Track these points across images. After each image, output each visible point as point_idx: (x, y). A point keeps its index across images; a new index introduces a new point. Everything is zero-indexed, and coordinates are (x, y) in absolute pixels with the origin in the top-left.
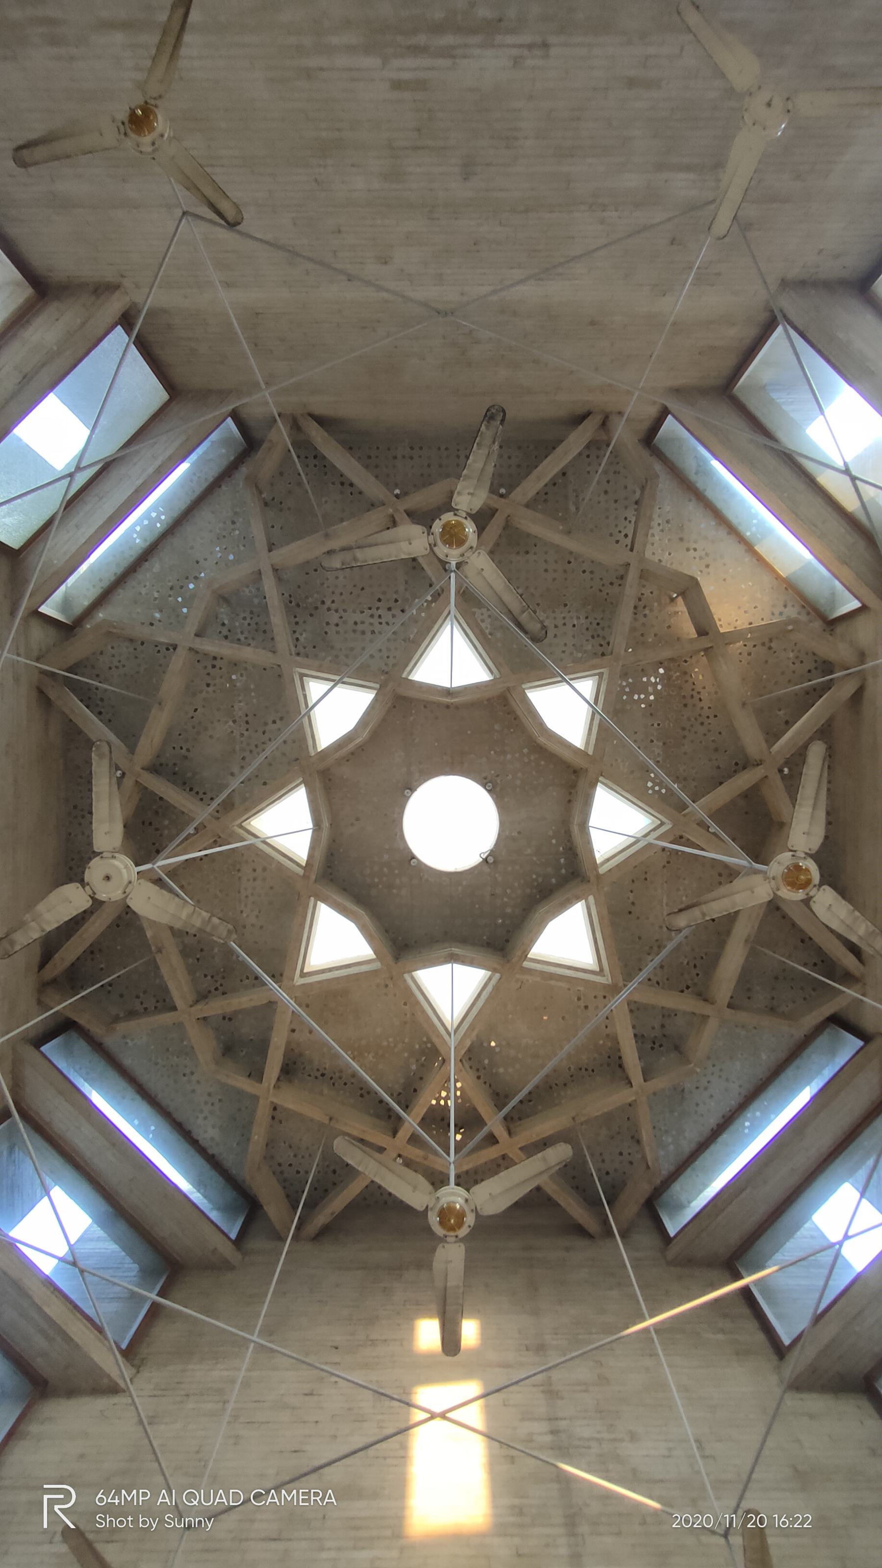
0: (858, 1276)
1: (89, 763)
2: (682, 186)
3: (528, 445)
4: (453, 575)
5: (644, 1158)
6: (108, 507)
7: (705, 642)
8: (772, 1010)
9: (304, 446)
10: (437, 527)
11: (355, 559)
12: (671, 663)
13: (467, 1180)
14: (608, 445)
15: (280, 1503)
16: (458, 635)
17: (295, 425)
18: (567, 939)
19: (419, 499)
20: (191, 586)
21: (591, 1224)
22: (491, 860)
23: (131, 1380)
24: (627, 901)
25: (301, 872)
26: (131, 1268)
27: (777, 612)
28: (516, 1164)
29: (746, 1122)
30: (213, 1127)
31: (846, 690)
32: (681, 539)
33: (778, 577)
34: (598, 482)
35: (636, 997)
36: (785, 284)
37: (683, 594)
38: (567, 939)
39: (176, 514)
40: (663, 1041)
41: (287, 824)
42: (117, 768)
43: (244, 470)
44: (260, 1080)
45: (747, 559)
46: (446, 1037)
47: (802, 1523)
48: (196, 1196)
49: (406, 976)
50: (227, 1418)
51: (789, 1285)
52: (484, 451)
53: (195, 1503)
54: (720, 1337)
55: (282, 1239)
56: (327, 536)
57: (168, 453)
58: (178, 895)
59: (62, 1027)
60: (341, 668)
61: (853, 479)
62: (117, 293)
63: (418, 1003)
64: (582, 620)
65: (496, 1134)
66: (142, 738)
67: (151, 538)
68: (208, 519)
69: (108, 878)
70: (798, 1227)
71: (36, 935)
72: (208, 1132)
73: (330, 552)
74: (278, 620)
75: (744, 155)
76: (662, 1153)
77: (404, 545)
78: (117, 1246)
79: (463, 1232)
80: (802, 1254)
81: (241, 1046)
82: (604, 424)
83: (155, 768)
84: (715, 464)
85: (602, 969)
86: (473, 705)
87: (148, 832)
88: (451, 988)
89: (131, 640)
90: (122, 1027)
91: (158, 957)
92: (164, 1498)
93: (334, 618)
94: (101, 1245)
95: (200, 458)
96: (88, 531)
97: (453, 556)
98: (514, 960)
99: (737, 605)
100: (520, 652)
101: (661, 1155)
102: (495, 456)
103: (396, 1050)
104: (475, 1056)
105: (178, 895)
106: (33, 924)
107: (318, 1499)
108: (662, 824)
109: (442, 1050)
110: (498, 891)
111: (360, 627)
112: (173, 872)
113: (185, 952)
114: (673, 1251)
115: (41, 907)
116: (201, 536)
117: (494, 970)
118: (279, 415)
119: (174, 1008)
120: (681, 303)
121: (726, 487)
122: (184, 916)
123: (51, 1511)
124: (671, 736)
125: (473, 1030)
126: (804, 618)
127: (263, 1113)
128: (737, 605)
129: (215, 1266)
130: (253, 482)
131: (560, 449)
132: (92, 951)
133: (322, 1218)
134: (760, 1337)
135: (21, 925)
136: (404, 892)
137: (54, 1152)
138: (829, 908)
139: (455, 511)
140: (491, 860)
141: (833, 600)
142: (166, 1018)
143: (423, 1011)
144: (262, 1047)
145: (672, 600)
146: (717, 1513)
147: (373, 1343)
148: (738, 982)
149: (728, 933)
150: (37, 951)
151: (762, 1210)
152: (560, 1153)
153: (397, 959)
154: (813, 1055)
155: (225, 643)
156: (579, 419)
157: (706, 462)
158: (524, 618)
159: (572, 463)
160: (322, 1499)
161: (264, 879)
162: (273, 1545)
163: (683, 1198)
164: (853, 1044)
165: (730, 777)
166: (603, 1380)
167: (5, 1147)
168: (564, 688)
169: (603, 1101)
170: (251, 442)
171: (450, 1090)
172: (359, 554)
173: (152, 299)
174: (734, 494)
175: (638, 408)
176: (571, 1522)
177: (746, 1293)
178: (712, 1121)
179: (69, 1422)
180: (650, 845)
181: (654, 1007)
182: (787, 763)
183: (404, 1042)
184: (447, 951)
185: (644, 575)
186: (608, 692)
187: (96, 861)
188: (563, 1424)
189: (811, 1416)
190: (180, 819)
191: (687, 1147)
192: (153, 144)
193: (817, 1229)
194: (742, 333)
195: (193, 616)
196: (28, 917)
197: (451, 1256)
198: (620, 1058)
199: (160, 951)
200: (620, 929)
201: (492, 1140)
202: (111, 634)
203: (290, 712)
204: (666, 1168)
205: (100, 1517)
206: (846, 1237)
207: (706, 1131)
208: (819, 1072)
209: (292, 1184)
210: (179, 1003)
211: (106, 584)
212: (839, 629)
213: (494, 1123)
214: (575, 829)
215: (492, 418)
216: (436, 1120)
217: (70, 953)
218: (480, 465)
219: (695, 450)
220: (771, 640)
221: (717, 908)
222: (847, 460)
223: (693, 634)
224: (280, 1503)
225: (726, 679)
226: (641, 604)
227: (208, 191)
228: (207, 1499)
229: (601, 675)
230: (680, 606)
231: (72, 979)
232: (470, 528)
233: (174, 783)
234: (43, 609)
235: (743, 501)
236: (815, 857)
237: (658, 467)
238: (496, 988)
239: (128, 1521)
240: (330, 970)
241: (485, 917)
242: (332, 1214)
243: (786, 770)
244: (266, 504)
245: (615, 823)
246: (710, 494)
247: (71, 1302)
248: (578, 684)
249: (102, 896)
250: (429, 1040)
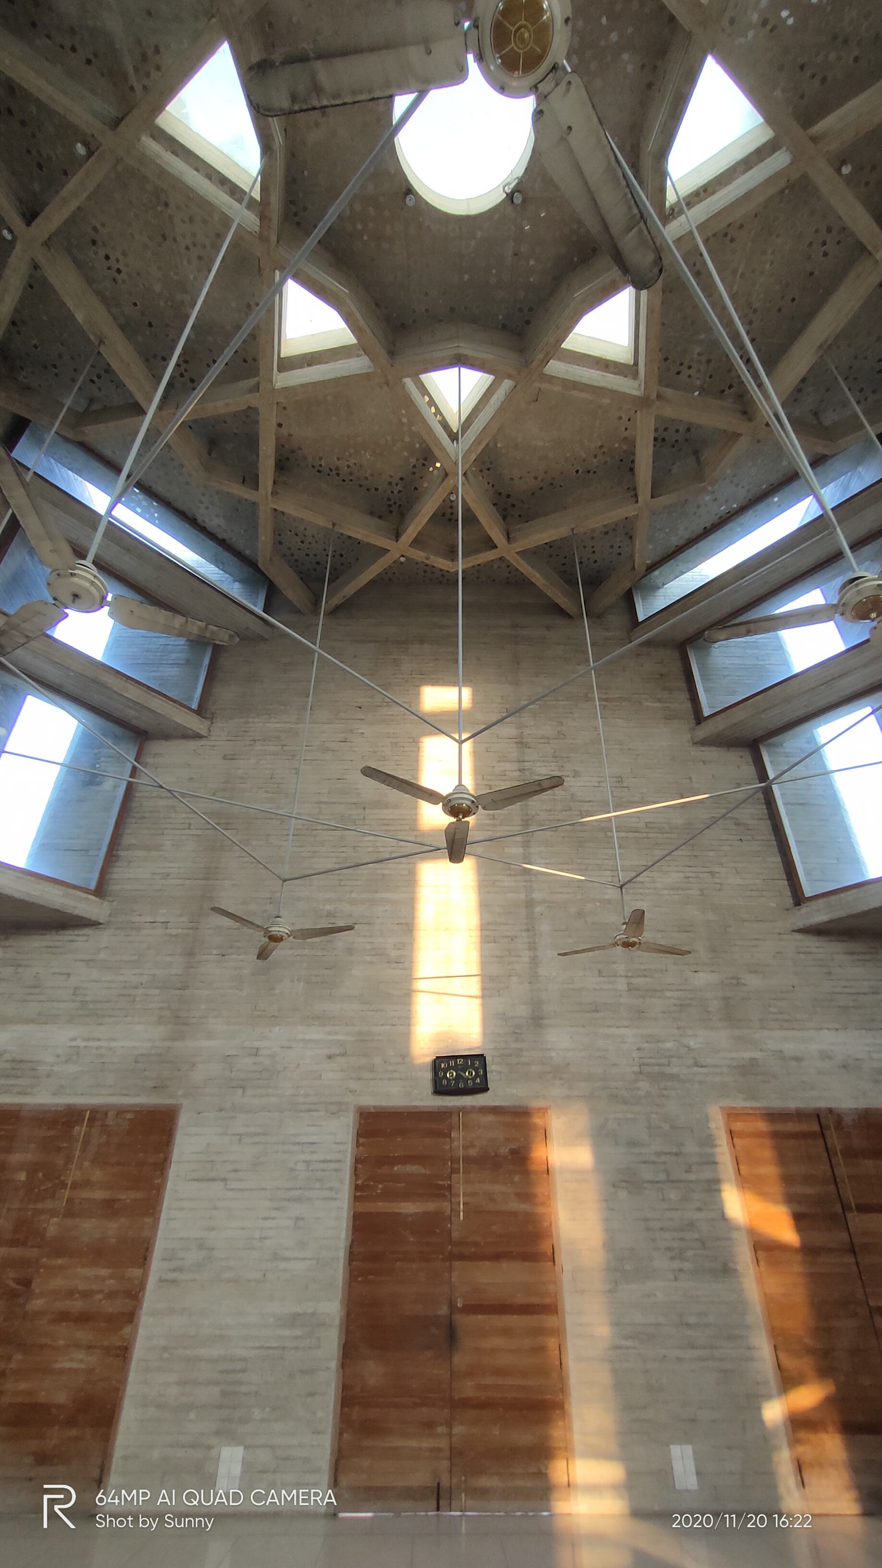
11: (317, 89)
15: (280, 1503)
30: (217, 516)
44: (256, 487)
47: (802, 1523)
51: (731, 670)
53: (195, 1503)
72: (215, 521)
91: (102, 350)
92: (164, 1498)
98: (535, 364)
103: (395, 449)
107: (318, 1499)
110: (524, 249)
123: (52, 1515)
125: (480, 444)
134: (688, 705)
144: (252, 442)
160: (322, 1500)
163: (659, 582)
166: (561, 735)
178: (707, 519)
183: (403, 441)
191: (676, 541)
198: (633, 461)
205: (100, 1518)
209: (303, 564)
224: (280, 1503)
228: (207, 1499)
239: (128, 1521)
242: (344, 597)
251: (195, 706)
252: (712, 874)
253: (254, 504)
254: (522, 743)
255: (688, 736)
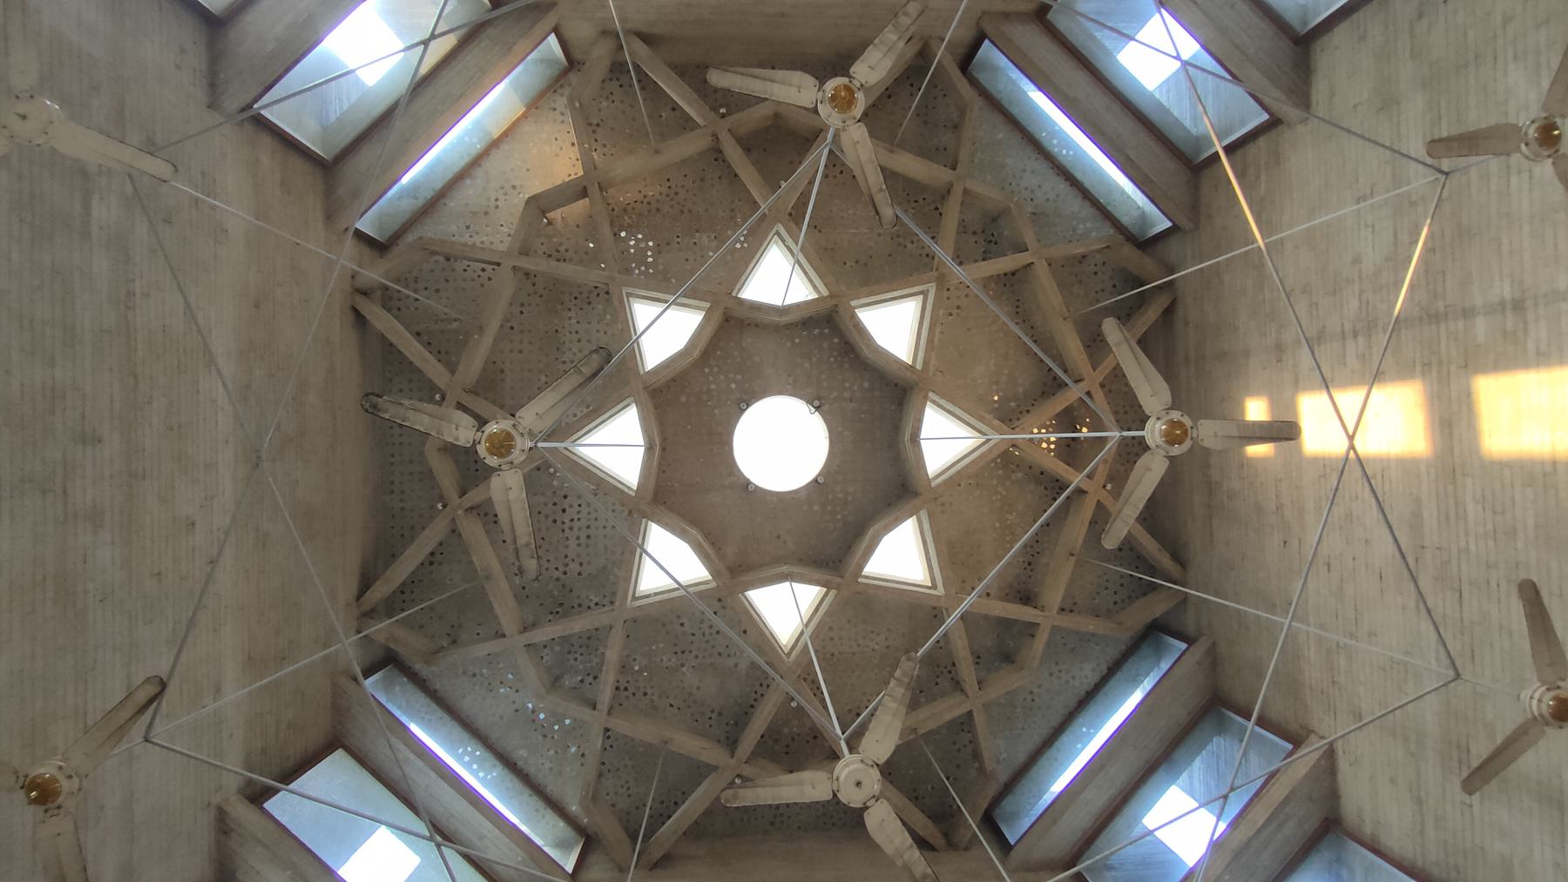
0: (1204, 47)
2: (105, 212)
3: (386, 370)
5: (1099, 251)
6: (460, 806)
7: (594, 190)
8: (956, 127)
9: (390, 607)
10: (493, 461)
11: (528, 545)
13: (1133, 415)
14: (387, 288)
16: (589, 439)
17: (369, 615)
18: (893, 326)
20: (542, 716)
21: (1164, 300)
22: (817, 403)
23: (1323, 738)
24: (855, 268)
25: (833, 592)
26: (1218, 744)
27: (561, 118)
29: (1063, 154)
31: (642, 49)
33: (524, 116)
36: (213, 105)
37: (544, 213)
38: (893, 326)
39: (465, 736)
40: (988, 233)
41: (785, 608)
42: (733, 782)
43: (418, 667)
46: (991, 444)
48: (1147, 684)
49: (933, 484)
50: (1353, 642)
51: (1214, 112)
52: (411, 414)
54: (1263, 178)
55: (1186, 597)
56: (488, 577)
58: (875, 709)
59: (990, 823)
61: (433, 37)
62: (228, 809)
64: (572, 314)
66: (703, 759)
68: (472, 702)
69: (858, 784)
71: (917, 853)
72: (1087, 674)
74: (578, 625)
75: (82, 144)
77: (512, 495)
79: (1187, 421)
81: (1002, 645)
82: (365, 293)
83: (732, 743)
84: (406, 180)
86: (662, 425)
87: (800, 745)
88: (944, 440)
89: (600, 775)
90: (989, 765)
91: (921, 732)
93: (574, 567)
94: (1196, 775)
95: (406, 713)
96: (486, 826)
97: (522, 443)
99: (555, 158)
100: (607, 376)
101: (1097, 235)
104: (1008, 417)
105: (875, 709)
106: (906, 857)
108: (778, 233)
109: (1002, 449)
110: (847, 395)
111: (583, 540)
114: (1184, 223)
115: (889, 849)
116: (487, 707)
117: (926, 398)
118: (359, 632)
119: (970, 713)
120: (235, 212)
121: (431, 168)
122: (895, 705)
126: (567, 91)
127: (1066, 621)
128: (555, 158)
129: (1213, 661)
131: (393, 339)
133: (1166, 562)
134: (1262, 141)
135: (906, 867)
136: (851, 489)
137: (1104, 833)
140: (817, 403)
141: (548, 61)
142: (979, 720)
144: (1006, 624)
145: (550, 223)
146: (1419, 179)
147: (1280, 507)
151: (1144, 137)
153: (916, 494)
154: (998, 88)
156: (360, 319)
157: (403, 190)
158: (587, 371)
162: (1466, 595)
163: (1136, 213)
164: (987, 50)
165: (729, 166)
167: (1108, 874)
170: (386, 660)
171: (1041, 437)
173: (234, 772)
174: (438, 160)
175: (347, 256)
176: (1434, 318)
177: (1229, 149)
178: (1063, 186)
179: (1370, 794)
182: (715, 109)
184: (908, 444)
185: (525, 252)
186: (647, 288)
187: (843, 798)
188: (1348, 327)
189: (1332, 95)
191: (1087, 210)
192: (70, 777)
193: (1160, 86)
194: (267, 150)
196: (899, 863)
199: (915, 730)
200: (883, 272)
202: (593, 797)
203: (675, 609)
208: (1014, 82)
210: (963, 709)
211: (541, 805)
212: (577, 55)
213: (1074, 393)
214: (785, 319)
215: (375, 407)
216: (1071, 452)
218: (426, 419)
219: (391, 199)
221: (875, 180)
222: (402, 46)
225: (634, 169)
226: (555, 254)
227: (125, 714)
229: (629, 295)
230: (556, 215)
231: (944, 816)
233: (746, 724)
236: (822, 81)
237: (410, 238)
238: (942, 396)
243: (723, 110)
244: (454, 642)
245: (777, 279)
246: (438, 185)
247: (1251, 800)
250: (994, 460)
251: (1290, 747)
252: (1507, 20)
254: (1319, 338)
255: (1300, 129)
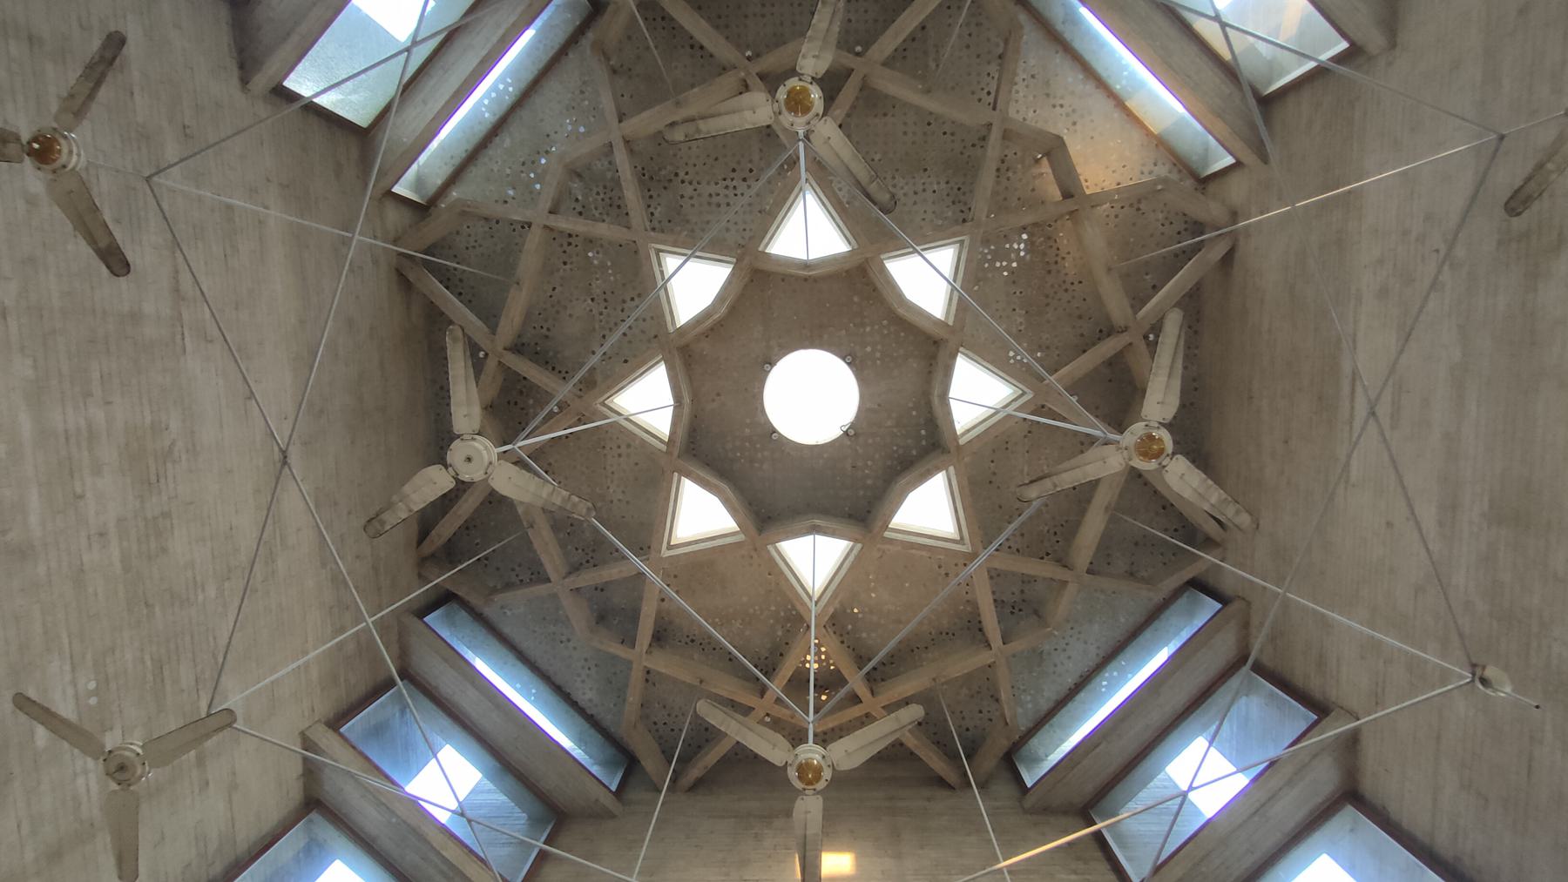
0: (1209, 821)
1: (444, 349)
4: (801, 144)
6: (454, 80)
7: (1070, 205)
8: (1131, 575)
10: (782, 94)
11: (698, 131)
12: (1033, 228)
13: (824, 739)
18: (928, 509)
19: (769, 62)
21: (952, 777)
22: (852, 432)
24: (987, 473)
26: (520, 818)
27: (1146, 170)
28: (876, 719)
29: (1103, 681)
31: (1216, 253)
32: (1048, 95)
33: (1148, 133)
34: (960, 36)
35: (996, 565)
37: (1047, 154)
39: (523, 85)
40: (1022, 607)
41: (648, 401)
43: (590, 35)
45: (1117, 115)
48: (577, 753)
49: (770, 547)
57: (512, 19)
59: (442, 599)
60: (697, 243)
63: (782, 573)
64: (943, 186)
65: (860, 693)
67: (500, 112)
68: (556, 92)
69: (469, 459)
70: (1152, 778)
72: (587, 694)
73: (673, 124)
74: (631, 194)
76: (1020, 710)
77: (748, 114)
78: (504, 798)
79: (821, 785)
80: (1150, 803)
81: (614, 613)
83: (518, 348)
85: (962, 538)
87: (510, 410)
88: (814, 559)
91: (530, 532)
97: (799, 124)
99: (1105, 164)
100: (877, 220)
102: (840, 16)
104: (838, 622)
105: (539, 476)
108: (1024, 393)
110: (860, 464)
111: (715, 200)
112: (538, 454)
113: (556, 527)
114: (1030, 801)
115: (407, 488)
121: (1095, 37)
122: (544, 495)
124: (1024, 304)
126: (1175, 176)
127: (637, 676)
128: (1105, 164)
129: (597, 815)
130: (602, 50)
132: (467, 527)
133: (695, 772)
135: (389, 506)
136: (765, 466)
138: (1181, 478)
139: (800, 76)
140: (852, 432)
141: (1206, 157)
142: (541, 590)
143: (787, 580)
144: (634, 616)
145: (1037, 161)
148: (1098, 549)
149: (1089, 502)
150: (414, 529)
152: (916, 712)
153: (760, 530)
154: (1171, 617)
155: (581, 220)
158: (873, 188)
159: (930, 17)
161: (628, 455)
163: (1041, 752)
165: (1094, 344)
168: (914, 260)
169: (962, 663)
172: (702, 125)
177: (1098, 836)
178: (1070, 681)
180: (1009, 416)
181: (1014, 574)
184: (808, 523)
185: (1006, 135)
190: (543, 397)
191: (1045, 706)
195: (546, 192)
197: (810, 807)
200: (982, 500)
201: (855, 699)
202: (465, 213)
204: (1024, 724)
206: (1191, 788)
207: (1064, 691)
208: (1177, 633)
211: (457, 161)
212: (1212, 187)
214: (936, 401)
217: (445, 529)
218: (824, 25)
220: (1139, 201)
221: (1070, 477)
223: (1058, 195)
225: (1091, 246)
226: (1004, 167)
229: (962, 242)
230: (1045, 167)
232: (816, 94)
233: (536, 362)
234: (397, 189)
235: (1112, 52)
236: (1169, 426)
237: (1023, 17)
238: (858, 558)
240: (696, 542)
241: (849, 488)
244: (614, 72)
246: (1078, 45)
247: (466, 847)
248: (930, 255)
249: (466, 477)
250: (794, 607)
253: (630, 662)
